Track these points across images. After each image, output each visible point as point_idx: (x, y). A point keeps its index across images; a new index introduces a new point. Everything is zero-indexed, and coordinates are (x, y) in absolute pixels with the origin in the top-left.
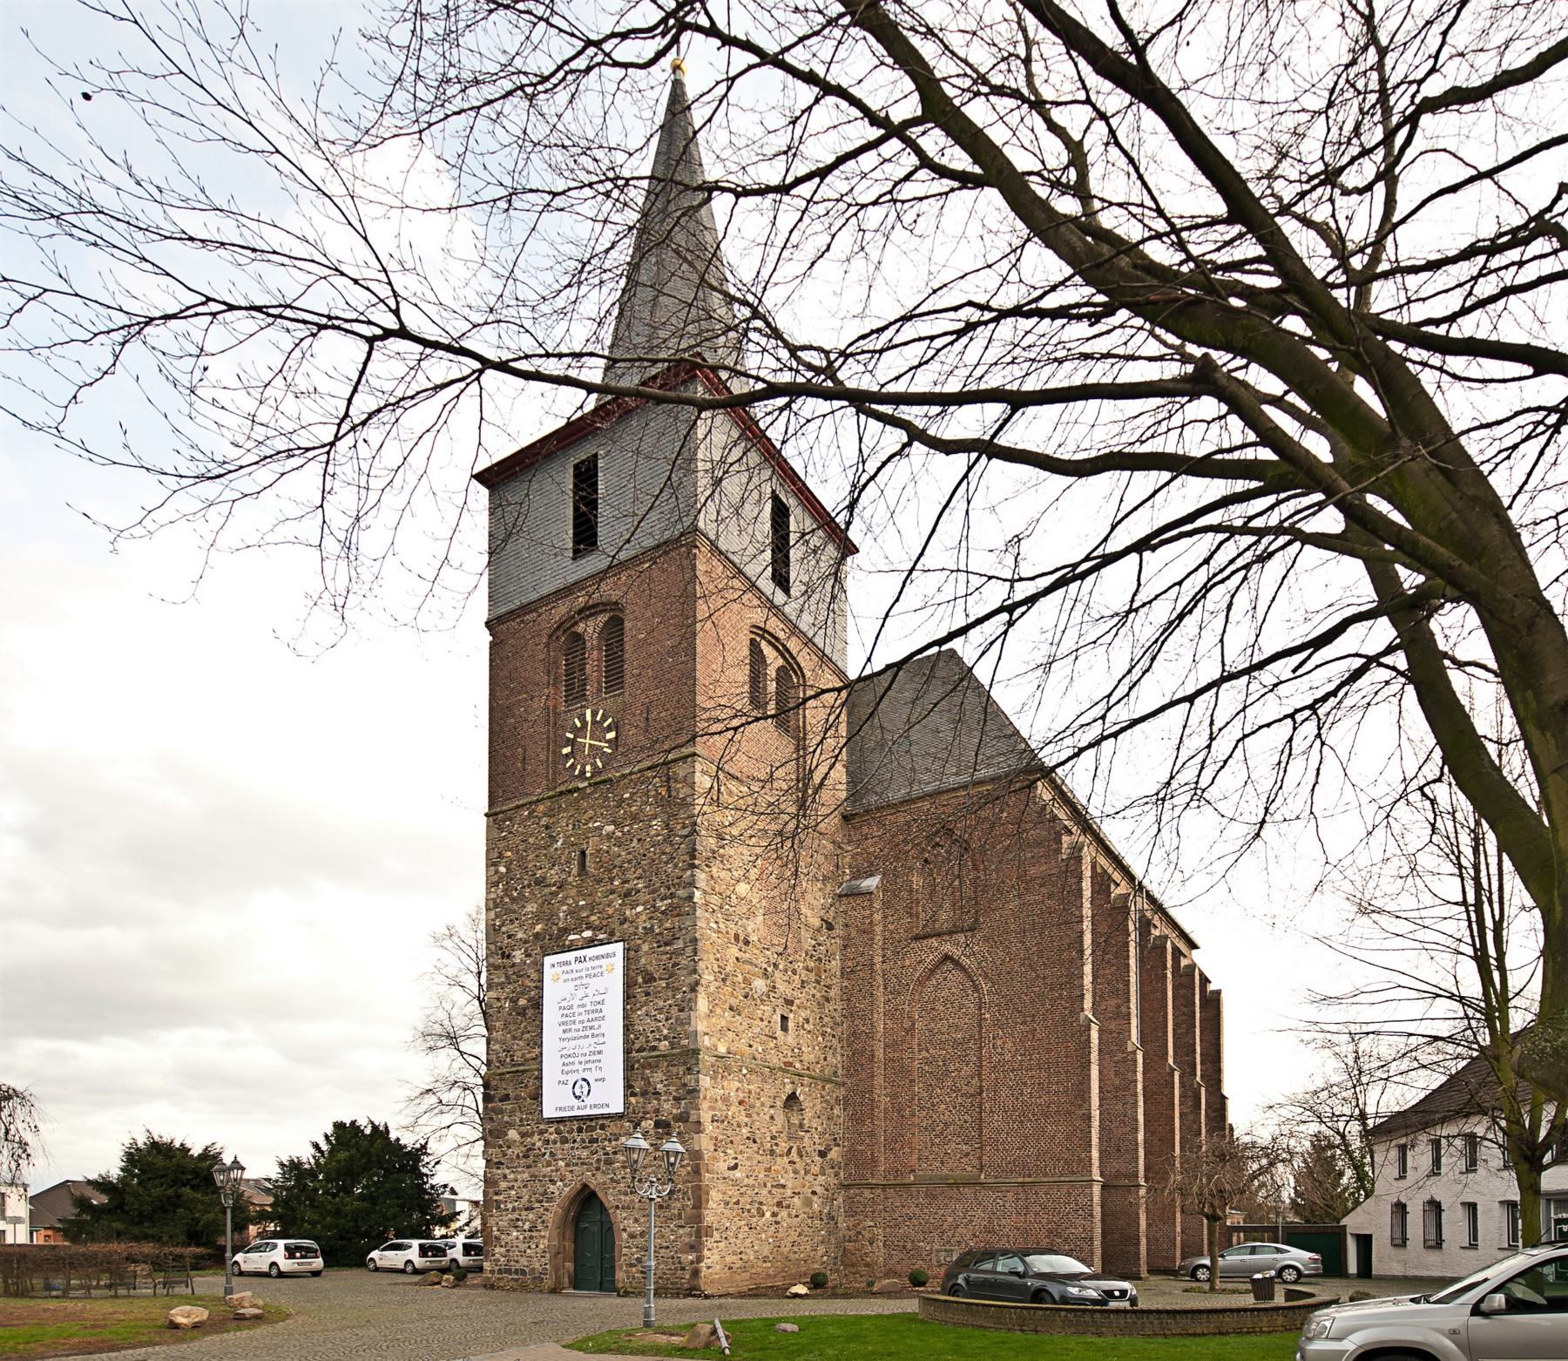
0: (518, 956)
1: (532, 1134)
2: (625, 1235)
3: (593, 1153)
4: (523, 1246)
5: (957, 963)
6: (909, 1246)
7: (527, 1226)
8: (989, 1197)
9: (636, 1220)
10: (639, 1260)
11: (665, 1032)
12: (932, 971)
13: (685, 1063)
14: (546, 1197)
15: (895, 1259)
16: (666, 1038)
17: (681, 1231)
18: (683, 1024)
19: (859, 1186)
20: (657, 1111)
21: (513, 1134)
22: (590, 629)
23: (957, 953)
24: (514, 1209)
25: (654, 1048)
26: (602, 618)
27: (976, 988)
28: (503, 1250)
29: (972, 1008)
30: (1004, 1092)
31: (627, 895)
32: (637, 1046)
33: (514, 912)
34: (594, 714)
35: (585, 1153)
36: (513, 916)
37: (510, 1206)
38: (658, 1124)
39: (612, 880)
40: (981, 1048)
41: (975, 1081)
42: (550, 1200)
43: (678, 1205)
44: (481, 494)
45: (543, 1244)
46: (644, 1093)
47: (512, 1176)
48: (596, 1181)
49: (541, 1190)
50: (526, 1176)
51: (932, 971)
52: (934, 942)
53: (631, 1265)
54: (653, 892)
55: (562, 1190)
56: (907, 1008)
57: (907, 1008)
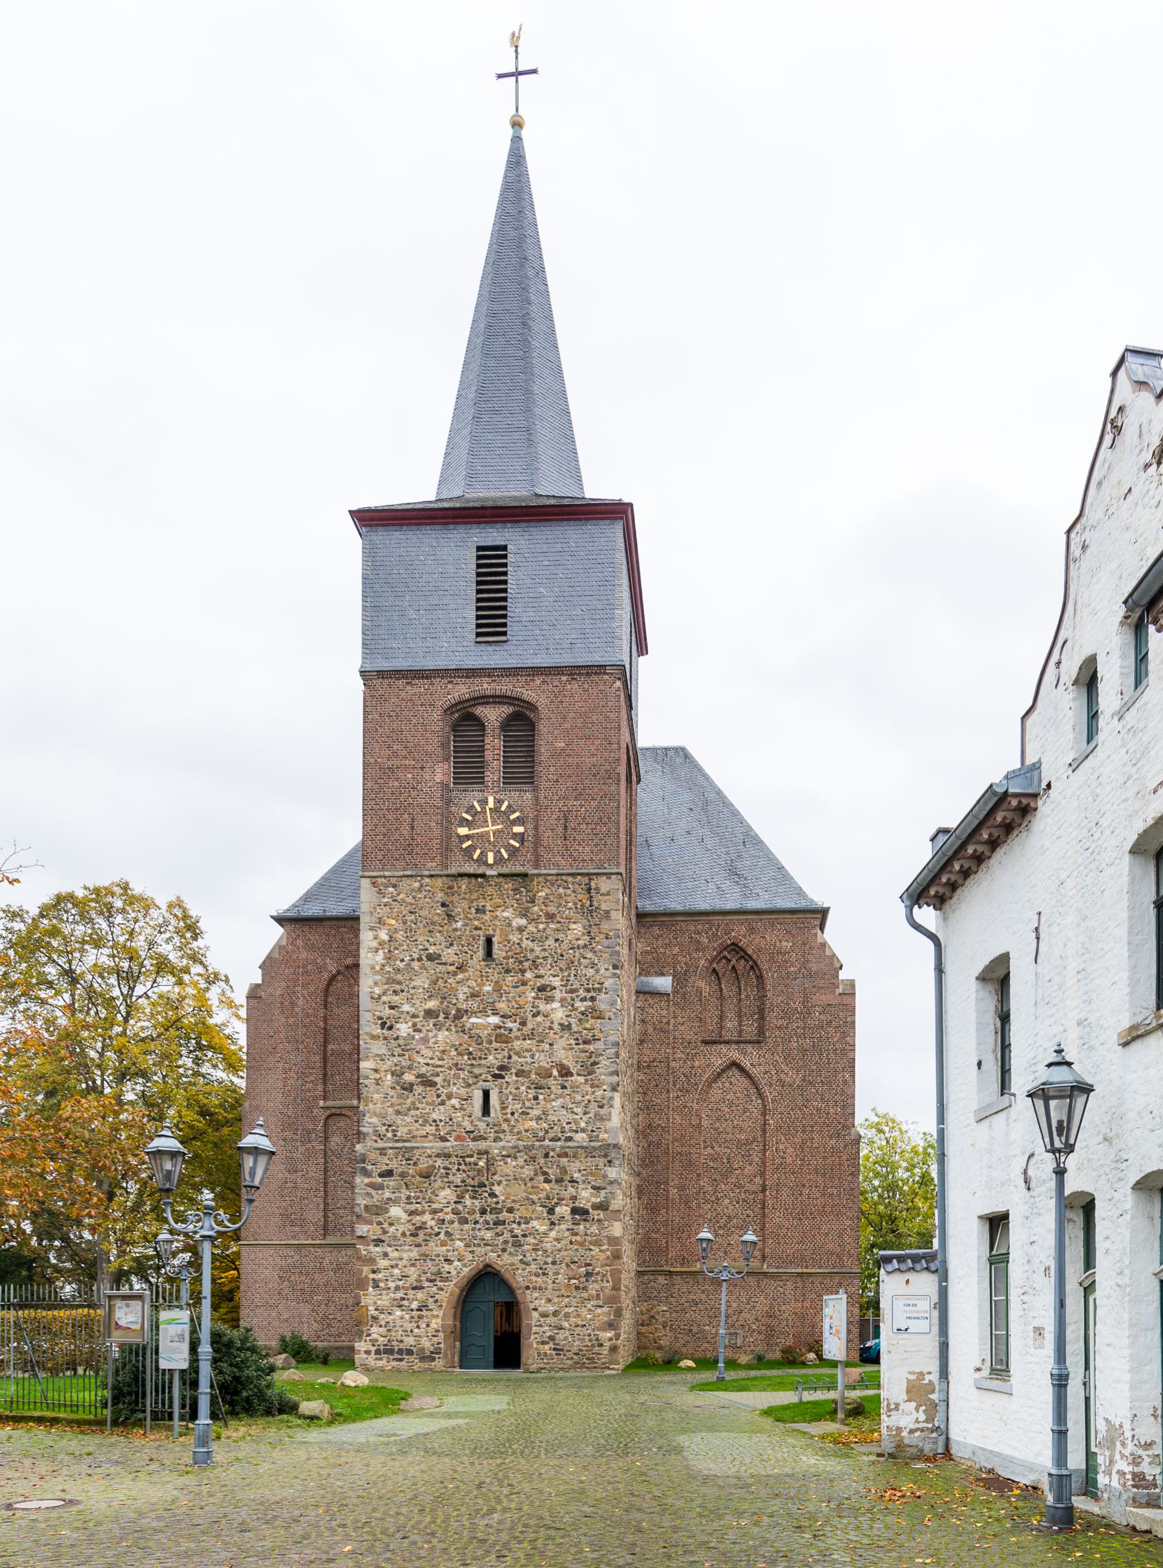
0: (404, 1029)
1: (423, 1212)
2: (535, 1314)
3: (498, 1235)
4: (409, 1326)
5: (742, 1069)
6: (695, 1329)
7: (415, 1305)
8: (771, 1286)
9: (549, 1301)
10: (552, 1338)
11: (583, 1125)
12: (719, 1075)
13: (606, 1156)
14: (438, 1276)
15: (682, 1342)
16: (583, 1130)
17: (599, 1311)
18: (602, 1119)
19: (654, 1273)
20: (574, 1198)
21: (396, 1211)
22: (493, 715)
23: (746, 1063)
24: (397, 1288)
25: (570, 1139)
26: (507, 710)
27: (761, 1095)
28: (383, 1330)
29: (756, 1113)
30: (785, 1192)
31: (542, 989)
32: (550, 1135)
33: (400, 983)
34: (499, 802)
35: (488, 1235)
36: (398, 987)
37: (392, 1285)
38: (575, 1211)
39: (523, 971)
40: (764, 1150)
41: (758, 1180)
42: (447, 1280)
43: (596, 1286)
44: (351, 540)
45: (436, 1324)
46: (559, 1181)
47: (396, 1254)
48: (504, 1262)
49: (434, 1269)
50: (414, 1254)
51: (719, 1075)
52: (724, 1048)
53: (543, 1343)
54: (572, 991)
55: (460, 1271)
56: (696, 1107)
57: (696, 1107)
